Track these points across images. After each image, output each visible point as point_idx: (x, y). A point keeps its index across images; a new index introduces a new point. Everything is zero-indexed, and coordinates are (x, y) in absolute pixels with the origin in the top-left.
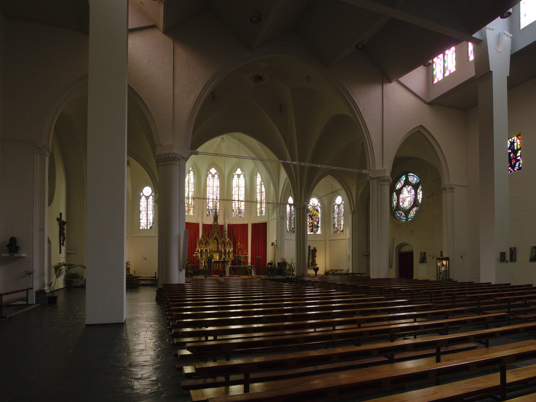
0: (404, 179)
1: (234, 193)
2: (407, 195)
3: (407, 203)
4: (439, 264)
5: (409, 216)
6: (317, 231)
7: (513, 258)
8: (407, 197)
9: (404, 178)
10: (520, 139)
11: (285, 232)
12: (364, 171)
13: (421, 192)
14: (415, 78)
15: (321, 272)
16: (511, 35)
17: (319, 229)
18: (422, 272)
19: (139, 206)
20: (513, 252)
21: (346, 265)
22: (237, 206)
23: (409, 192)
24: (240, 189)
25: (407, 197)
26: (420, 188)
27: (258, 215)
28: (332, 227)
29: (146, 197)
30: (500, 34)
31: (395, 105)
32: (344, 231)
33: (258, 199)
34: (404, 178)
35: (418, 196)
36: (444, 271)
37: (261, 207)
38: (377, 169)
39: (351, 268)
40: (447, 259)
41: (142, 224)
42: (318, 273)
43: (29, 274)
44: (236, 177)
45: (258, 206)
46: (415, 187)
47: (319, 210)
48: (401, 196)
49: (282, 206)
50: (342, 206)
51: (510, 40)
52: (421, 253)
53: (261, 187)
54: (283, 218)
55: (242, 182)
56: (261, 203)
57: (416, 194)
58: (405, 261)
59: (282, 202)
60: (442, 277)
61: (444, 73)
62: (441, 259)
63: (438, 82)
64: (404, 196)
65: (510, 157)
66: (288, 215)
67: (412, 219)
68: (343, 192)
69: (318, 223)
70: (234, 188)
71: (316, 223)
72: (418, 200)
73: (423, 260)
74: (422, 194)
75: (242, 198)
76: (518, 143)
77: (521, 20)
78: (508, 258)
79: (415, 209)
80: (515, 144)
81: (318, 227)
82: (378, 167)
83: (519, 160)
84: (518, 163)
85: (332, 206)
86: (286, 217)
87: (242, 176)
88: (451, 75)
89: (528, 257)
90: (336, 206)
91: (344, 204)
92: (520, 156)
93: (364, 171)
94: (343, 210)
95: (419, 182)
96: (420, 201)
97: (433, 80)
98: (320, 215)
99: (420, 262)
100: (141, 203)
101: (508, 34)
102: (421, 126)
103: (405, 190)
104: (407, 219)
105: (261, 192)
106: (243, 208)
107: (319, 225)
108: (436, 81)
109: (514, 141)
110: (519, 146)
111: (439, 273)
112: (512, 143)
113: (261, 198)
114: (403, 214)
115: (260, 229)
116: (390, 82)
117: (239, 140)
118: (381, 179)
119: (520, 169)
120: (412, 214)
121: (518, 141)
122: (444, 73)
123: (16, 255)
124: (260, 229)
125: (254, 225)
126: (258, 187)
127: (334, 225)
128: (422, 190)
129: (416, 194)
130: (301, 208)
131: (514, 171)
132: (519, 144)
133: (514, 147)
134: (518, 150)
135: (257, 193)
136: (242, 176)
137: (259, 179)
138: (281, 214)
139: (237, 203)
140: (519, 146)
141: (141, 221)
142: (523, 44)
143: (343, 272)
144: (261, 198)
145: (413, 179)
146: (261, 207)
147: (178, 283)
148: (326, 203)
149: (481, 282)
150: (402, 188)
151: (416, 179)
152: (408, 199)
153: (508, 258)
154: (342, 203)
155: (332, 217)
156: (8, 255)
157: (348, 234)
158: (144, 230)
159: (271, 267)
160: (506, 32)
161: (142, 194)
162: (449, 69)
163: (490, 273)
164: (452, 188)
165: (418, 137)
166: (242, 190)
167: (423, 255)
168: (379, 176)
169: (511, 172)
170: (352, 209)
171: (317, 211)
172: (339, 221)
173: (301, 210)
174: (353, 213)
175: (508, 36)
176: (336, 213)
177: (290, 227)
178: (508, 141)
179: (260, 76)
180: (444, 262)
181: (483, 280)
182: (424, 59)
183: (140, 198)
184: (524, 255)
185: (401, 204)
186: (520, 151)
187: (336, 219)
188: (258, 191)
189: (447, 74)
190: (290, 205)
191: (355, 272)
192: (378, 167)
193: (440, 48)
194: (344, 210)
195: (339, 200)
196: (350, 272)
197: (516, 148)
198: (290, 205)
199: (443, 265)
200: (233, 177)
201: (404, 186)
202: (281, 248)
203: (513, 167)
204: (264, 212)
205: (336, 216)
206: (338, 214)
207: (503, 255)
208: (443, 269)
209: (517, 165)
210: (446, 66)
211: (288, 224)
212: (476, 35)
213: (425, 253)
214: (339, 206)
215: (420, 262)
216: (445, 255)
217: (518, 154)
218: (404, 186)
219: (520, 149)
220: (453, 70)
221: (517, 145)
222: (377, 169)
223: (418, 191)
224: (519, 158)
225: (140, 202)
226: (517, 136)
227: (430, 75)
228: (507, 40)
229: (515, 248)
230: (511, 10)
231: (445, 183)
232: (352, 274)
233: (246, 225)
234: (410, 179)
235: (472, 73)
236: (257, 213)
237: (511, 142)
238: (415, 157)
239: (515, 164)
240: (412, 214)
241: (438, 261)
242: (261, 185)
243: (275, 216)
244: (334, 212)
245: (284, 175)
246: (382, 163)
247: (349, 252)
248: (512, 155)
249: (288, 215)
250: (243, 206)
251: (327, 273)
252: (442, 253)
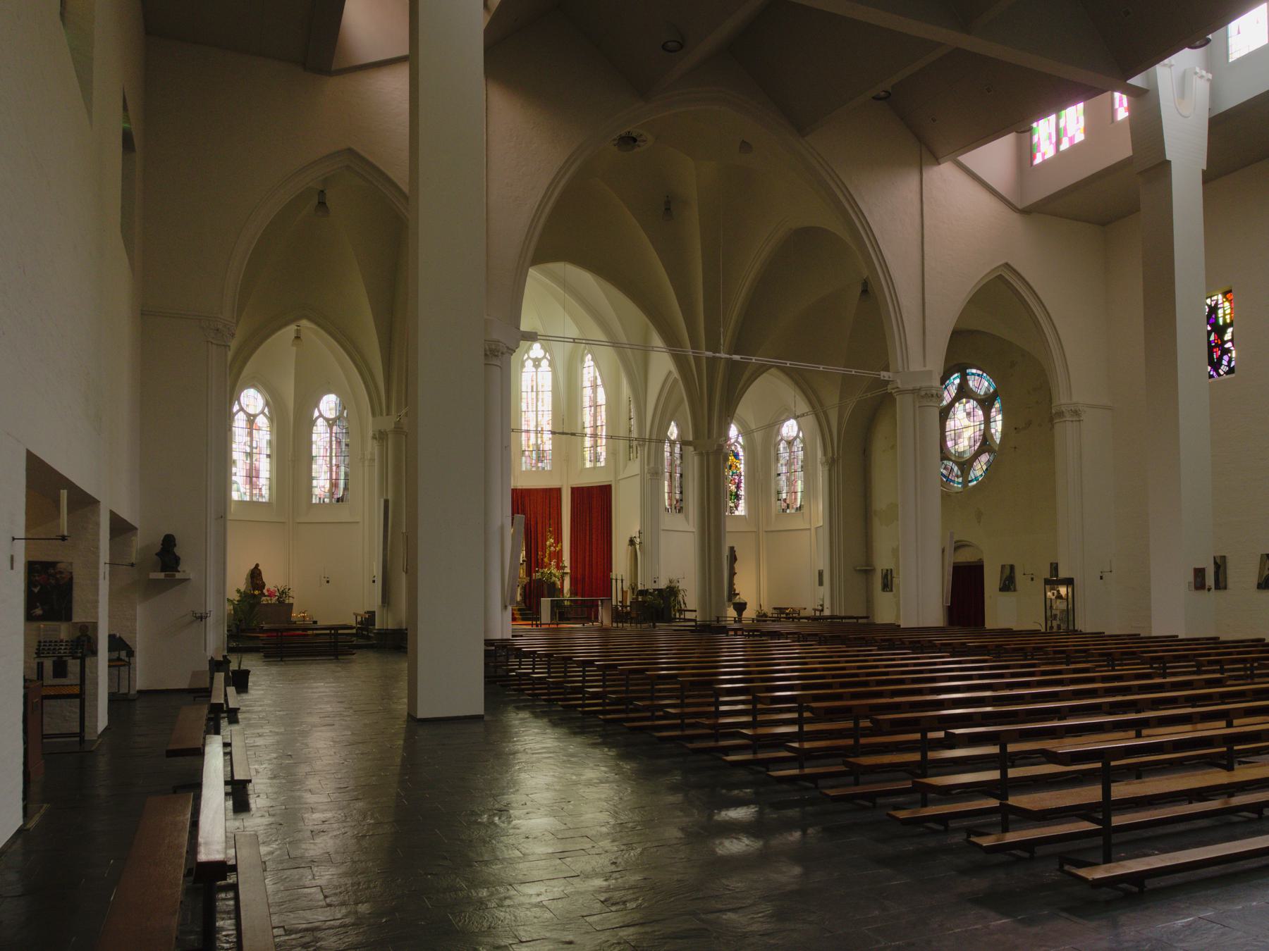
0: (957, 381)
1: (524, 408)
2: (966, 422)
3: (966, 443)
4: (1049, 594)
5: (972, 476)
6: (736, 507)
7: (1220, 584)
8: (965, 427)
9: (955, 380)
10: (1230, 301)
11: (662, 510)
12: (885, 375)
13: (999, 417)
14: (993, 158)
15: (749, 613)
16: (1210, 76)
17: (742, 502)
18: (1002, 612)
19: (310, 443)
20: (1220, 565)
21: (814, 597)
22: (532, 441)
23: (968, 414)
24: (540, 396)
25: (965, 427)
26: (997, 405)
27: (588, 465)
28: (773, 499)
29: (327, 420)
30: (1185, 72)
31: (948, 213)
32: (805, 510)
33: (587, 424)
34: (955, 380)
35: (993, 425)
36: (1062, 611)
37: (595, 446)
38: (912, 369)
39: (827, 604)
40: (1069, 582)
41: (316, 491)
42: (746, 614)
43: (201, 618)
44: (529, 364)
45: (588, 442)
46: (986, 403)
47: (741, 453)
48: (950, 424)
49: (653, 444)
50: (798, 445)
51: (1207, 85)
52: (1003, 567)
53: (595, 392)
54: (657, 473)
55: (545, 377)
56: (594, 436)
57: (988, 420)
58: (966, 586)
59: (654, 437)
60: (1059, 627)
61: (1058, 142)
62: (1053, 581)
63: (1045, 162)
64: (958, 425)
65: (1209, 343)
66: (667, 469)
67: (980, 483)
68: (803, 407)
69: (738, 487)
70: (524, 395)
71: (733, 488)
72: (992, 435)
73: (1008, 584)
74: (1004, 420)
75: (546, 422)
76: (1225, 312)
77: (1231, 41)
78: (1210, 580)
79: (984, 458)
80: (1220, 312)
81: (737, 497)
82: (915, 366)
83: (1228, 351)
84: (1226, 358)
85: (785, 443)
86: (663, 473)
87: (545, 363)
88: (1075, 148)
89: (1254, 579)
90: (782, 445)
91: (803, 441)
92: (1232, 341)
93: (885, 375)
94: (801, 454)
95: (995, 391)
96: (997, 438)
97: (1033, 157)
98: (742, 467)
99: (1001, 590)
100: (314, 437)
101: (1204, 73)
102: (1007, 265)
103: (960, 410)
104: (966, 482)
105: (595, 406)
106: (548, 446)
107: (742, 492)
108: (1038, 160)
109: (1216, 304)
110: (1228, 317)
111: (1050, 616)
112: (1214, 310)
113: (595, 420)
114: (956, 469)
115: (594, 503)
116: (937, 160)
117: (564, 284)
118: (923, 393)
119: (1231, 371)
120: (979, 469)
121: (1227, 304)
122: (1058, 142)
123: (178, 576)
124: (594, 503)
125: (575, 491)
126: (587, 392)
127: (779, 493)
128: (1003, 410)
129: (988, 420)
130: (712, 457)
131: (1219, 375)
132: (1228, 311)
133: (1217, 318)
134: (1226, 326)
135: (583, 408)
136: (545, 363)
137: (589, 371)
138: (652, 465)
139: (532, 435)
140: (1228, 317)
141: (315, 483)
142: (1236, 95)
143: (803, 614)
144: (595, 420)
145: (981, 383)
146: (595, 446)
147: (499, 637)
148: (758, 436)
149: (1154, 634)
150: (951, 405)
151: (986, 384)
152: (968, 433)
153: (1210, 580)
154: (797, 436)
155: (773, 474)
156: (162, 576)
157: (819, 512)
158: (322, 504)
159: (644, 602)
160: (1198, 70)
161: (316, 414)
162: (1070, 135)
163: (1175, 615)
164: (1076, 413)
165: (1000, 292)
166: (547, 398)
167: (1007, 572)
168: (918, 386)
169: (1211, 377)
170: (830, 455)
171: (736, 456)
172: (791, 483)
173: (711, 458)
174: (831, 463)
175: (1202, 77)
176: (782, 461)
177: (670, 498)
178: (1200, 297)
179: (634, 135)
180: (1063, 590)
181: (1159, 628)
182: (1015, 118)
183: (312, 423)
184: (1244, 574)
185: (950, 444)
186: (1230, 330)
187: (783, 478)
188: (587, 402)
189: (1065, 145)
190: (672, 443)
191: (837, 613)
192: (915, 366)
193: (1055, 100)
194: (805, 455)
195: (790, 428)
196: (827, 613)
197: (1221, 322)
198: (672, 443)
199: (1059, 597)
200: (523, 366)
201: (957, 399)
202: (656, 548)
203: (1216, 365)
204: (602, 458)
205: (784, 469)
206: (789, 463)
207: (1199, 573)
208: (1061, 605)
209: (1225, 362)
210: (1062, 125)
211: (666, 489)
212: (1136, 81)
213: (1012, 567)
214: (790, 443)
215: (1001, 590)
216: (1063, 574)
217: (1228, 337)
218: (957, 399)
219: (1231, 325)
220: (1080, 137)
221: (1225, 315)
222: (912, 369)
223: (993, 414)
224: (1229, 345)
225: (311, 433)
226: (1225, 294)
227: (1025, 151)
228: (1200, 87)
229: (1224, 558)
230: (1210, 36)
231: (1062, 399)
232: (832, 617)
233: (559, 491)
234: (971, 383)
235: (1122, 149)
236: (583, 459)
237: (1210, 307)
238: (996, 336)
239: (1220, 359)
240: (979, 469)
241: (1048, 587)
242: (594, 387)
243: (635, 467)
244: (778, 460)
245: (662, 365)
246: (918, 351)
247: (823, 563)
248: (1212, 338)
249: (667, 469)
250: (547, 443)
251: (762, 617)
252: (1054, 568)
